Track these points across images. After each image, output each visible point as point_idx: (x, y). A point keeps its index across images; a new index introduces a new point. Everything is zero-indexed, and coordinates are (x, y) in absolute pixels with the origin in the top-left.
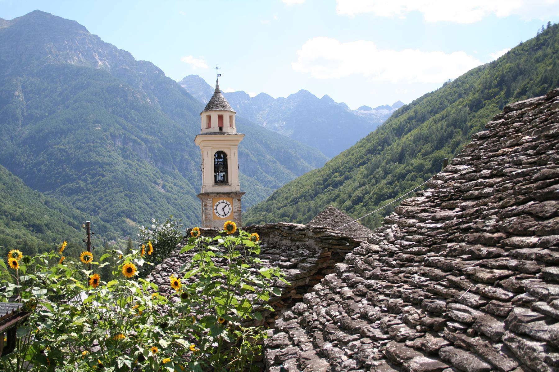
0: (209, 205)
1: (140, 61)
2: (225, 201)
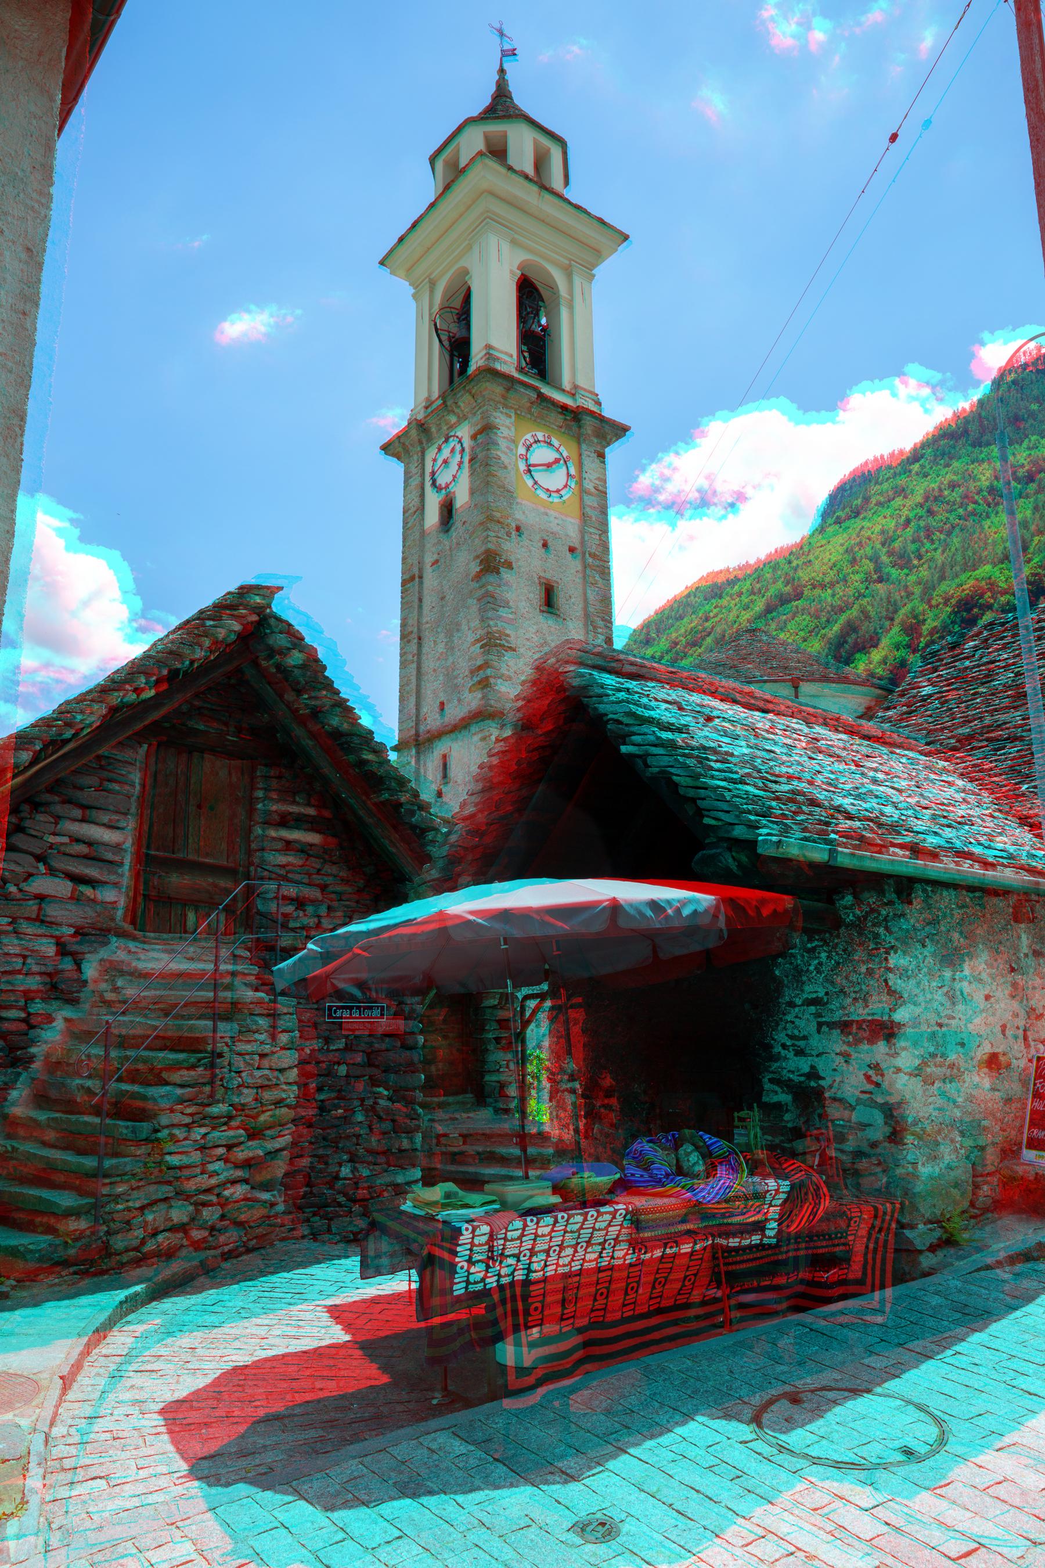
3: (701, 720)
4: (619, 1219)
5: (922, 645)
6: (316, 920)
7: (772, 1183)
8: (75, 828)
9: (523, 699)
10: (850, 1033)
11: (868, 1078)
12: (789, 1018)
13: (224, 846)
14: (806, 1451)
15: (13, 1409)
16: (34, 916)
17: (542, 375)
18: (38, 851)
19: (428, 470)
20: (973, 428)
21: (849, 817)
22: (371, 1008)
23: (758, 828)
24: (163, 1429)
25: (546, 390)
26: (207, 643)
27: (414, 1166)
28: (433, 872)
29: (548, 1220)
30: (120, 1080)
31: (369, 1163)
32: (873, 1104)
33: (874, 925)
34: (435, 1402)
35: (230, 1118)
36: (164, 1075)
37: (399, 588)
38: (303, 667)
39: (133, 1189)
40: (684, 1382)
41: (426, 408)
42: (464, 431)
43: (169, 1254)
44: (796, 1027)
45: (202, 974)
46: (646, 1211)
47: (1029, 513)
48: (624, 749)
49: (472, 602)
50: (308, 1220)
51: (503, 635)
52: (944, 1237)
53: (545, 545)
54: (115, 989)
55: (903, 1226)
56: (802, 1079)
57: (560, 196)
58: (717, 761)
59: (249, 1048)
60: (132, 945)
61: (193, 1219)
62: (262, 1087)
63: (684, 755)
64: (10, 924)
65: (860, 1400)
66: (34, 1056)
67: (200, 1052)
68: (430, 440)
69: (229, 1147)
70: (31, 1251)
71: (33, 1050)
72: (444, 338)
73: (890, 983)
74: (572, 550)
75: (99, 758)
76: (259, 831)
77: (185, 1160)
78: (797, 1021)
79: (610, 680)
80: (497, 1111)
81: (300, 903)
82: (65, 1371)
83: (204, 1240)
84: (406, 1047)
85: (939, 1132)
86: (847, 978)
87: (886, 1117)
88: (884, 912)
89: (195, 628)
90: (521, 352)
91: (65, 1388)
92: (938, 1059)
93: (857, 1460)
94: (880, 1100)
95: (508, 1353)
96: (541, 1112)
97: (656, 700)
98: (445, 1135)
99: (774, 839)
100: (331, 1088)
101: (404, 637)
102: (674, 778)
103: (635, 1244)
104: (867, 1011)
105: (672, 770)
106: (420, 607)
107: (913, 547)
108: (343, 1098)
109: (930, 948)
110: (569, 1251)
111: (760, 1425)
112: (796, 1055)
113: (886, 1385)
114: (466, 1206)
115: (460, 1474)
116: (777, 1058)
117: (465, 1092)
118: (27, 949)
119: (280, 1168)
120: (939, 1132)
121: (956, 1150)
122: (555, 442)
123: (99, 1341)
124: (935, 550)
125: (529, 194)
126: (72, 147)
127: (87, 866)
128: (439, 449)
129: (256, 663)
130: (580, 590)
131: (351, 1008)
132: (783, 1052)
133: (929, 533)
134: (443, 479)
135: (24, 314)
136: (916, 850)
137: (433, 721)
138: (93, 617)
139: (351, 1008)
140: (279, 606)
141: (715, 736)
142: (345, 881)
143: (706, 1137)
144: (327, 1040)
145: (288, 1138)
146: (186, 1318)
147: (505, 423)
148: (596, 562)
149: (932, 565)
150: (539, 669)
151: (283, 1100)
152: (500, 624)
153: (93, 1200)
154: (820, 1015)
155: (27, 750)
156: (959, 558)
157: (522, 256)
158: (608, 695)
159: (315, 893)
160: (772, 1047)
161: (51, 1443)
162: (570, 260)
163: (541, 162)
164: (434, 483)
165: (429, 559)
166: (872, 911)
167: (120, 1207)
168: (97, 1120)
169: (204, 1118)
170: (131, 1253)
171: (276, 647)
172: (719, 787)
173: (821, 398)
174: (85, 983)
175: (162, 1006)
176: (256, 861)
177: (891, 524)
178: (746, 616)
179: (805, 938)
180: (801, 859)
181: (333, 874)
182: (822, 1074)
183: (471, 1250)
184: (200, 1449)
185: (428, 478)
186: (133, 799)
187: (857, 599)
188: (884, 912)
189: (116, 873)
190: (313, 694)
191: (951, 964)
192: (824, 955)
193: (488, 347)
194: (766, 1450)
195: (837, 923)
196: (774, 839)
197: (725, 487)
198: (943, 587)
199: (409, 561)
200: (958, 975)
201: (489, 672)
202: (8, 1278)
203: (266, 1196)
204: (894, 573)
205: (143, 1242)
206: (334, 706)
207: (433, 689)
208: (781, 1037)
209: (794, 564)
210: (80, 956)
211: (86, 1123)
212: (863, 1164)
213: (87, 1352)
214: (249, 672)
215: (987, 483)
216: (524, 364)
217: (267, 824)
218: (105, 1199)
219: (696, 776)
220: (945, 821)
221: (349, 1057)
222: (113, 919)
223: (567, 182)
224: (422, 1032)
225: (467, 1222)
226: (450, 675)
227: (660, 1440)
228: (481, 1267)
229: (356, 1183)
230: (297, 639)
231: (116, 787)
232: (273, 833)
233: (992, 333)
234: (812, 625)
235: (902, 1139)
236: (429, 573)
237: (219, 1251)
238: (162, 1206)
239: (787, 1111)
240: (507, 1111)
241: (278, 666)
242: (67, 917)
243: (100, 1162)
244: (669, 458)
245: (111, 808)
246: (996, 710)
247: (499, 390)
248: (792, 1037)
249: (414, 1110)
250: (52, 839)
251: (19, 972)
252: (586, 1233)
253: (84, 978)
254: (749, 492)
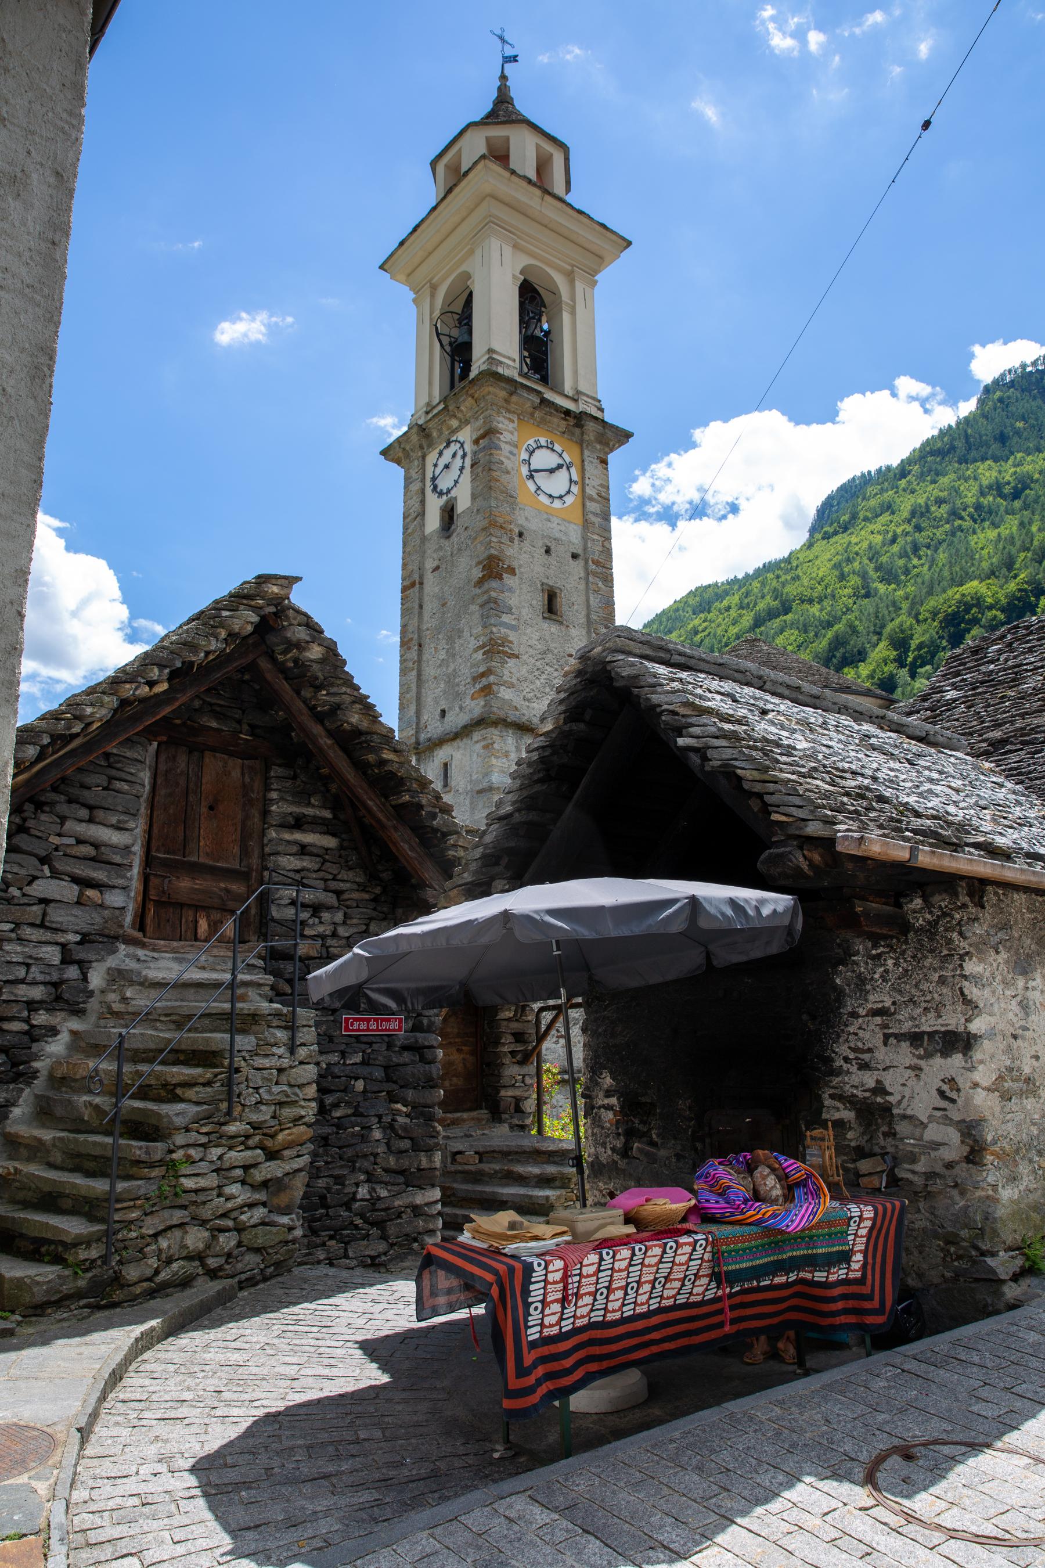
3: (757, 713)
4: (699, 1250)
5: (909, 660)
6: (332, 927)
7: (854, 1210)
8: (82, 829)
9: (565, 691)
10: (921, 1045)
11: (942, 1093)
12: (851, 1029)
13: (236, 850)
14: (936, 1520)
15: (28, 1470)
16: (38, 922)
17: (544, 380)
18: (43, 853)
19: (429, 475)
20: (960, 444)
21: (918, 815)
22: (389, 1020)
23: (835, 824)
24: (197, 1492)
25: (549, 395)
26: (223, 634)
27: (433, 1186)
28: (465, 875)
29: (625, 1253)
30: (133, 1097)
31: (386, 1184)
32: (948, 1121)
33: (946, 930)
34: (496, 1455)
35: (248, 1137)
36: (179, 1091)
37: (399, 595)
38: (322, 661)
39: (146, 1215)
40: (779, 1434)
41: (427, 413)
42: (466, 435)
43: (185, 1283)
44: (860, 1039)
45: (217, 985)
46: (727, 1241)
47: (1015, 528)
48: (681, 741)
49: (474, 608)
50: (324, 1244)
51: (505, 641)
52: (1027, 1265)
53: (548, 551)
54: (124, 1000)
55: (983, 1254)
56: (867, 1094)
57: (563, 201)
58: (781, 754)
59: (266, 1062)
60: (141, 953)
61: (208, 1247)
62: (281, 1104)
63: (748, 747)
64: (12, 931)
65: (981, 1457)
66: (38, 1071)
67: (216, 1067)
68: (431, 445)
69: (246, 1168)
70: (38, 1283)
71: (36, 1065)
72: (446, 340)
73: (966, 992)
74: (575, 556)
75: (107, 756)
76: (273, 834)
77: (202, 1183)
78: (861, 1033)
79: (662, 670)
80: (512, 1127)
81: (316, 909)
82: (82, 1422)
83: (221, 1268)
84: (423, 1060)
85: (1017, 1151)
86: (916, 986)
87: (963, 1135)
88: (958, 916)
89: (208, 619)
90: (522, 358)
91: (84, 1441)
92: (1015, 1073)
93: (1000, 1534)
94: (956, 1117)
95: (581, 1401)
96: (559, 1128)
97: (710, 691)
98: (460, 1153)
99: (855, 834)
100: (348, 1104)
101: (405, 644)
102: (739, 771)
103: (716, 1277)
104: (940, 1021)
105: (736, 763)
106: (420, 614)
107: (901, 562)
108: (362, 1115)
109: (1004, 956)
110: (647, 1287)
111: (876, 1488)
112: (859, 1069)
113: (1006, 1438)
114: (536, 1238)
115: (547, 1549)
116: (839, 1072)
117: (478, 1107)
118: (30, 957)
119: (298, 1188)
120: (1017, 1151)
121: (1034, 1171)
122: (558, 448)
123: (115, 1384)
124: (922, 565)
125: (531, 198)
126: (99, 70)
127: (95, 869)
128: (441, 454)
129: (273, 659)
130: (584, 598)
131: (368, 1020)
132: (845, 1066)
133: (916, 548)
134: (444, 484)
135: (54, 243)
136: (991, 850)
137: (434, 728)
138: (89, 623)
139: (368, 1020)
140: (298, 598)
141: (773, 729)
142: (362, 888)
143: (782, 1158)
144: (343, 1055)
145: (307, 1158)
146: (207, 1356)
147: (507, 427)
148: (599, 568)
149: (919, 580)
150: (584, 658)
151: (302, 1117)
152: (503, 630)
153: (104, 1227)
154: (887, 1027)
155: (34, 744)
156: (946, 573)
157: (525, 261)
158: (662, 685)
159: (331, 899)
160: (833, 1060)
161: (73, 1510)
162: (573, 266)
163: (543, 165)
164: (435, 488)
165: (430, 564)
166: (945, 914)
167: (133, 1234)
168: (109, 1140)
169: (221, 1137)
170: (145, 1284)
171: (294, 639)
172: (790, 780)
173: (814, 408)
174: (91, 994)
175: (174, 1018)
176: (271, 865)
177: (878, 539)
178: (734, 630)
179: (870, 944)
180: (884, 858)
181: (349, 879)
182: (889, 1089)
183: (545, 1288)
184: (241, 1516)
185: (428, 483)
186: (142, 800)
187: (844, 613)
188: (958, 916)
189: (124, 877)
190: (333, 690)
191: (1024, 972)
192: (890, 962)
193: (491, 351)
194: (894, 1520)
195: (905, 928)
196: (855, 834)
197: (722, 493)
198: (932, 603)
199: (410, 567)
200: (1031, 984)
201: (492, 679)
202: (13, 1312)
203: (285, 1220)
204: (882, 588)
205: (157, 1272)
206: (354, 702)
207: (434, 695)
208: (843, 1049)
209: (782, 579)
210: (87, 965)
211: (95, 1143)
212: (938, 1185)
213: (103, 1398)
214: (264, 664)
215: (974, 500)
216: (525, 369)
217: (283, 826)
218: (117, 1226)
219: (766, 769)
220: (1006, 822)
221: (364, 1071)
222: (122, 926)
223: (568, 189)
224: (441, 1046)
225: (538, 1256)
226: (450, 680)
227: (768, 1507)
228: (556, 1307)
229: (374, 1204)
230: (314, 629)
231: (125, 787)
232: (287, 836)
233: (984, 346)
234: (801, 639)
235: (982, 1157)
236: (430, 579)
237: (236, 1279)
238: (178, 1233)
239: (850, 1128)
240: (522, 1127)
241: (296, 661)
242: (73, 922)
243: (113, 1186)
244: (660, 469)
245: (120, 808)
246: (1027, 713)
247: (503, 394)
248: (854, 1050)
249: (434, 1127)
250: (55, 840)
251: (22, 981)
252: (665, 1268)
253: (91, 987)
254: (743, 504)
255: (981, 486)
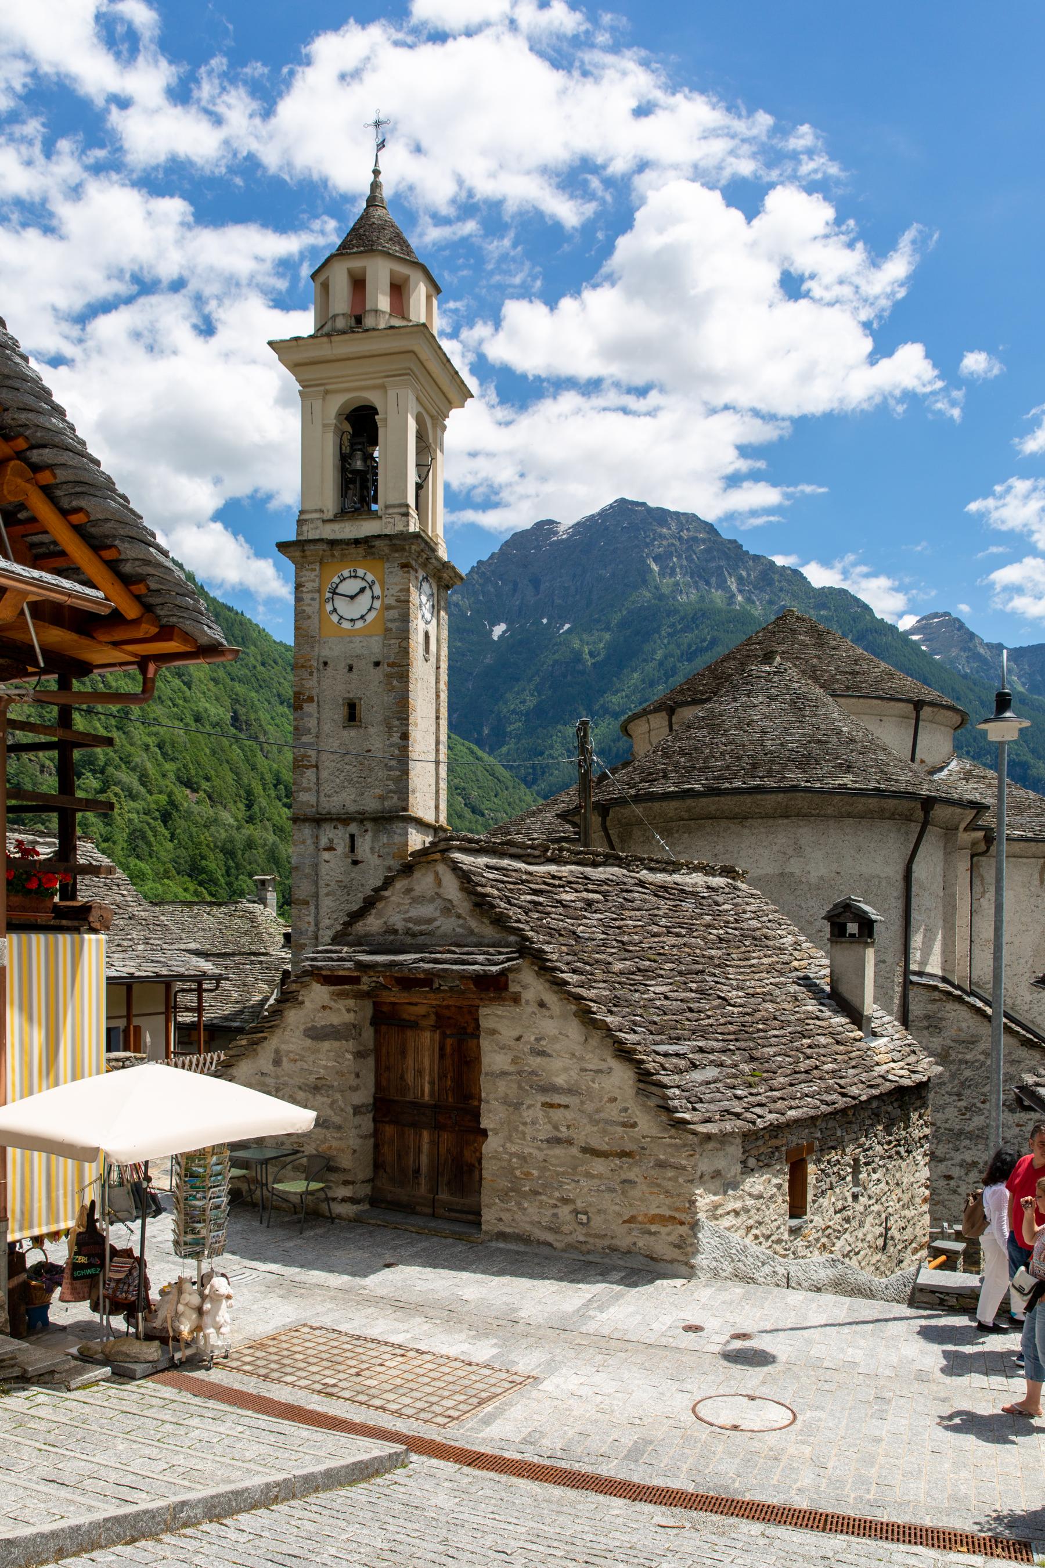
0: (309, 586)
1: (823, 588)
2: (361, 572)
255: (702, 175)
